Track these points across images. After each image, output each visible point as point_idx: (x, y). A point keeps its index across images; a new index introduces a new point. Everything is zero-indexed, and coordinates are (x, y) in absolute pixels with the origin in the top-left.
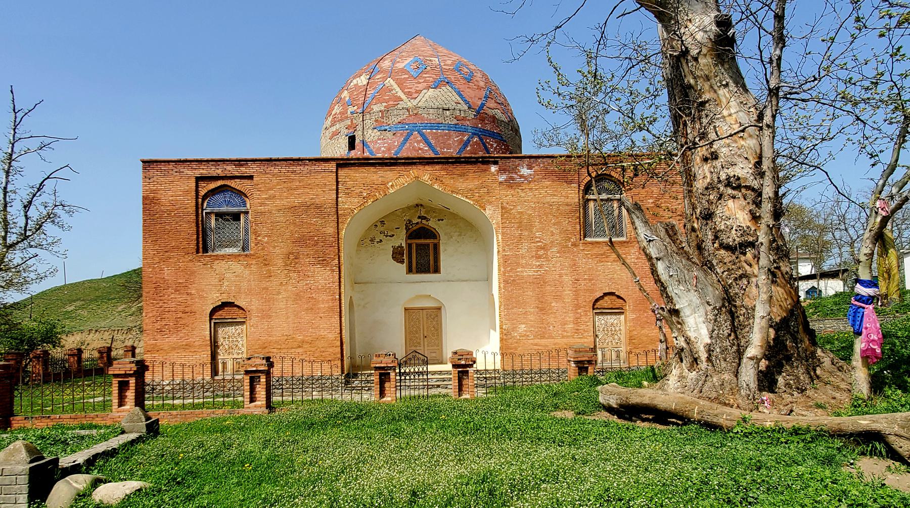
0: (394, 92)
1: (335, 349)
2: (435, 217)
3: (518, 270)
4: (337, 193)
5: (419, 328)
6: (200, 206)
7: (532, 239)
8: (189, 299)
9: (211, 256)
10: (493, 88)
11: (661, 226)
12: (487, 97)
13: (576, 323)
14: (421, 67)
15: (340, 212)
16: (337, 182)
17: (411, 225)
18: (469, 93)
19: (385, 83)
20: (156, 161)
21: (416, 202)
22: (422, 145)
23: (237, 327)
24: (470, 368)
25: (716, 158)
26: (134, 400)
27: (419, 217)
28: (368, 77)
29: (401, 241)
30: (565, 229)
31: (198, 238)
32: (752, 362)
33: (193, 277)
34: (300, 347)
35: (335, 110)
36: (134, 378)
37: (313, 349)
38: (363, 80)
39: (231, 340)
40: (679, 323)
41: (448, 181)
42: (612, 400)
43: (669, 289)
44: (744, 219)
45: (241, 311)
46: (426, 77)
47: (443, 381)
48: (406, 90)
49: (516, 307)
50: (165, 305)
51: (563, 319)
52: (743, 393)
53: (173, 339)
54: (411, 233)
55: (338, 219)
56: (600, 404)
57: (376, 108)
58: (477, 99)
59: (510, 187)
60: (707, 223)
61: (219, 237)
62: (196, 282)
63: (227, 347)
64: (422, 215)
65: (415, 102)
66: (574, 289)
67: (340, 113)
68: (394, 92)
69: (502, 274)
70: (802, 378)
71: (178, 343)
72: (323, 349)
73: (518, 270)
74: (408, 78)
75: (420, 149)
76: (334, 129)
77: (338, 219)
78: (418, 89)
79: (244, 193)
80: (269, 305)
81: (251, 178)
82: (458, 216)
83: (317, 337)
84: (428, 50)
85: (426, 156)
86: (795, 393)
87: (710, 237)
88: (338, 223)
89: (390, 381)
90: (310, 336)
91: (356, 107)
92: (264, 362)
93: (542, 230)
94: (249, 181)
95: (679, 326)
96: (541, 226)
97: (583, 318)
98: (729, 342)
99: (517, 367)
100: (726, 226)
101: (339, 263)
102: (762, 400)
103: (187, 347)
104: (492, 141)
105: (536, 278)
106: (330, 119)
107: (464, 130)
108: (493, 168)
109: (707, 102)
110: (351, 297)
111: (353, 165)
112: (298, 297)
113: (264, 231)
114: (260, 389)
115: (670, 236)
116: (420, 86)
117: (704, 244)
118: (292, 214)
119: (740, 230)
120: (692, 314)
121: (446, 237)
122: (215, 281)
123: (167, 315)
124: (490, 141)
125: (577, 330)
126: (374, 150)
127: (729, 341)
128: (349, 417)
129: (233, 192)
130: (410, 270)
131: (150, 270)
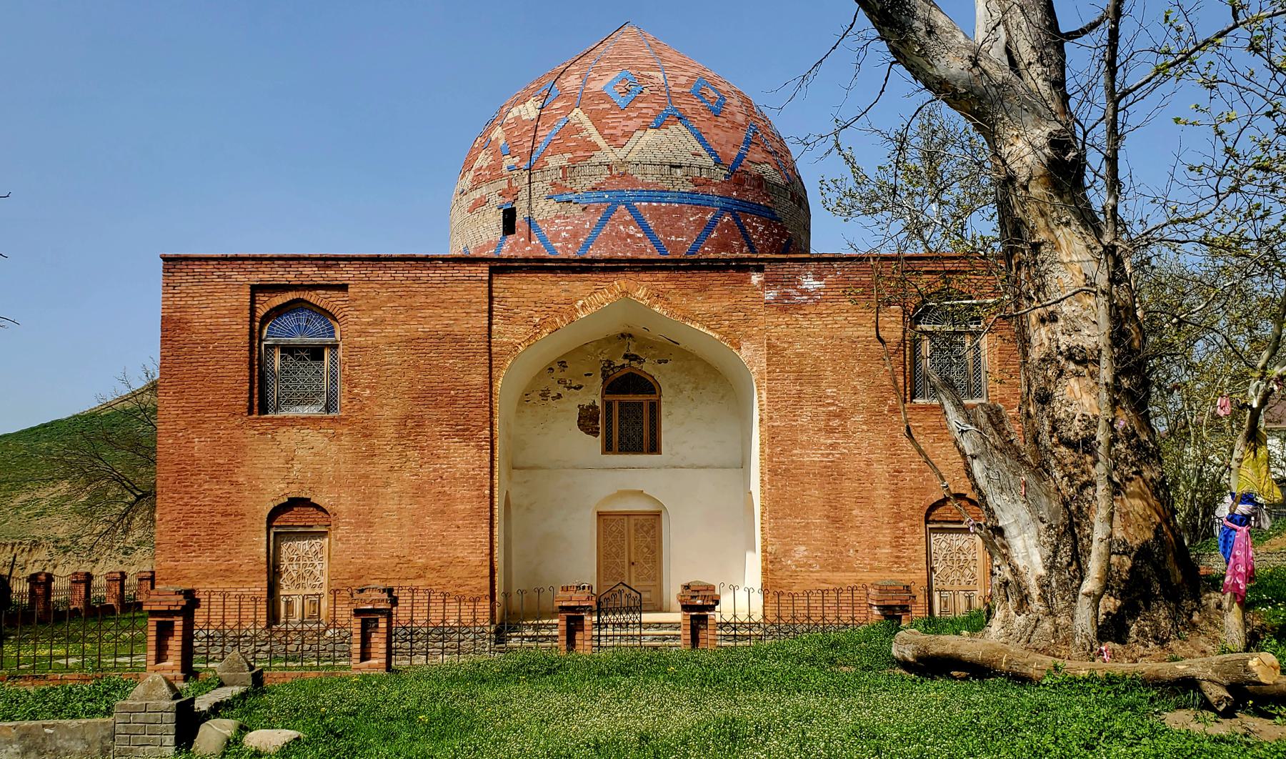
1: (480, 580)
2: (654, 356)
3: (795, 452)
4: (490, 318)
5: (622, 547)
6: (256, 335)
7: (819, 399)
8: (234, 491)
9: (273, 419)
10: (760, 124)
11: (982, 410)
12: (748, 142)
13: (897, 546)
14: (634, 90)
15: (494, 350)
16: (491, 298)
17: (612, 369)
18: (717, 136)
20: (186, 259)
21: (621, 330)
23: (313, 542)
24: (710, 611)
25: (1055, 320)
26: (180, 653)
27: (626, 357)
28: (540, 105)
29: (594, 397)
30: (878, 382)
31: (251, 388)
32: (1088, 600)
33: (242, 455)
34: (420, 577)
35: (479, 160)
36: (181, 618)
37: (443, 581)
38: (529, 110)
39: (301, 562)
40: (1004, 546)
41: (676, 299)
42: (907, 652)
44: (1091, 405)
45: (321, 514)
46: (641, 108)
47: (664, 640)
48: (606, 132)
49: (790, 515)
50: (194, 502)
51: (873, 538)
52: (1078, 641)
53: (206, 559)
54: (612, 384)
55: (491, 360)
56: (894, 658)
57: (553, 162)
58: (730, 146)
59: (784, 310)
60: (1043, 409)
61: (287, 387)
62: (246, 463)
63: (294, 575)
64: (632, 352)
65: (621, 153)
66: (893, 487)
67: (489, 167)
68: (585, 133)
69: (767, 458)
70: (1163, 624)
71: (212, 565)
72: (459, 581)
73: (795, 452)
74: (611, 109)
75: (629, 236)
76: (477, 194)
77: (491, 360)
78: (627, 129)
79: (331, 314)
80: (368, 505)
81: (343, 288)
82: (692, 354)
83: (450, 559)
84: (644, 55)
85: (642, 257)
86: (1151, 644)
87: (1046, 428)
89: (583, 630)
90: (439, 559)
91: (517, 159)
92: (385, 596)
94: (341, 294)
95: (1004, 551)
96: (835, 377)
97: (909, 538)
98: (1069, 574)
99: (787, 614)
100: (1066, 413)
101: (492, 435)
102: (1101, 651)
103: (228, 574)
104: (756, 222)
105: (825, 467)
106: (470, 176)
107: (707, 203)
108: (756, 278)
109: (1042, 243)
110: (507, 492)
111: (518, 270)
112: (419, 492)
113: (365, 378)
114: (376, 640)
115: (993, 424)
116: (632, 125)
117: (1040, 436)
118: (413, 352)
119: (1084, 420)
120: (1020, 535)
121: (672, 391)
122: (278, 463)
124: (753, 221)
125: (898, 557)
126: (549, 236)
127: (1069, 572)
128: (536, 672)
129: (313, 311)
130: (608, 448)
131: (170, 441)
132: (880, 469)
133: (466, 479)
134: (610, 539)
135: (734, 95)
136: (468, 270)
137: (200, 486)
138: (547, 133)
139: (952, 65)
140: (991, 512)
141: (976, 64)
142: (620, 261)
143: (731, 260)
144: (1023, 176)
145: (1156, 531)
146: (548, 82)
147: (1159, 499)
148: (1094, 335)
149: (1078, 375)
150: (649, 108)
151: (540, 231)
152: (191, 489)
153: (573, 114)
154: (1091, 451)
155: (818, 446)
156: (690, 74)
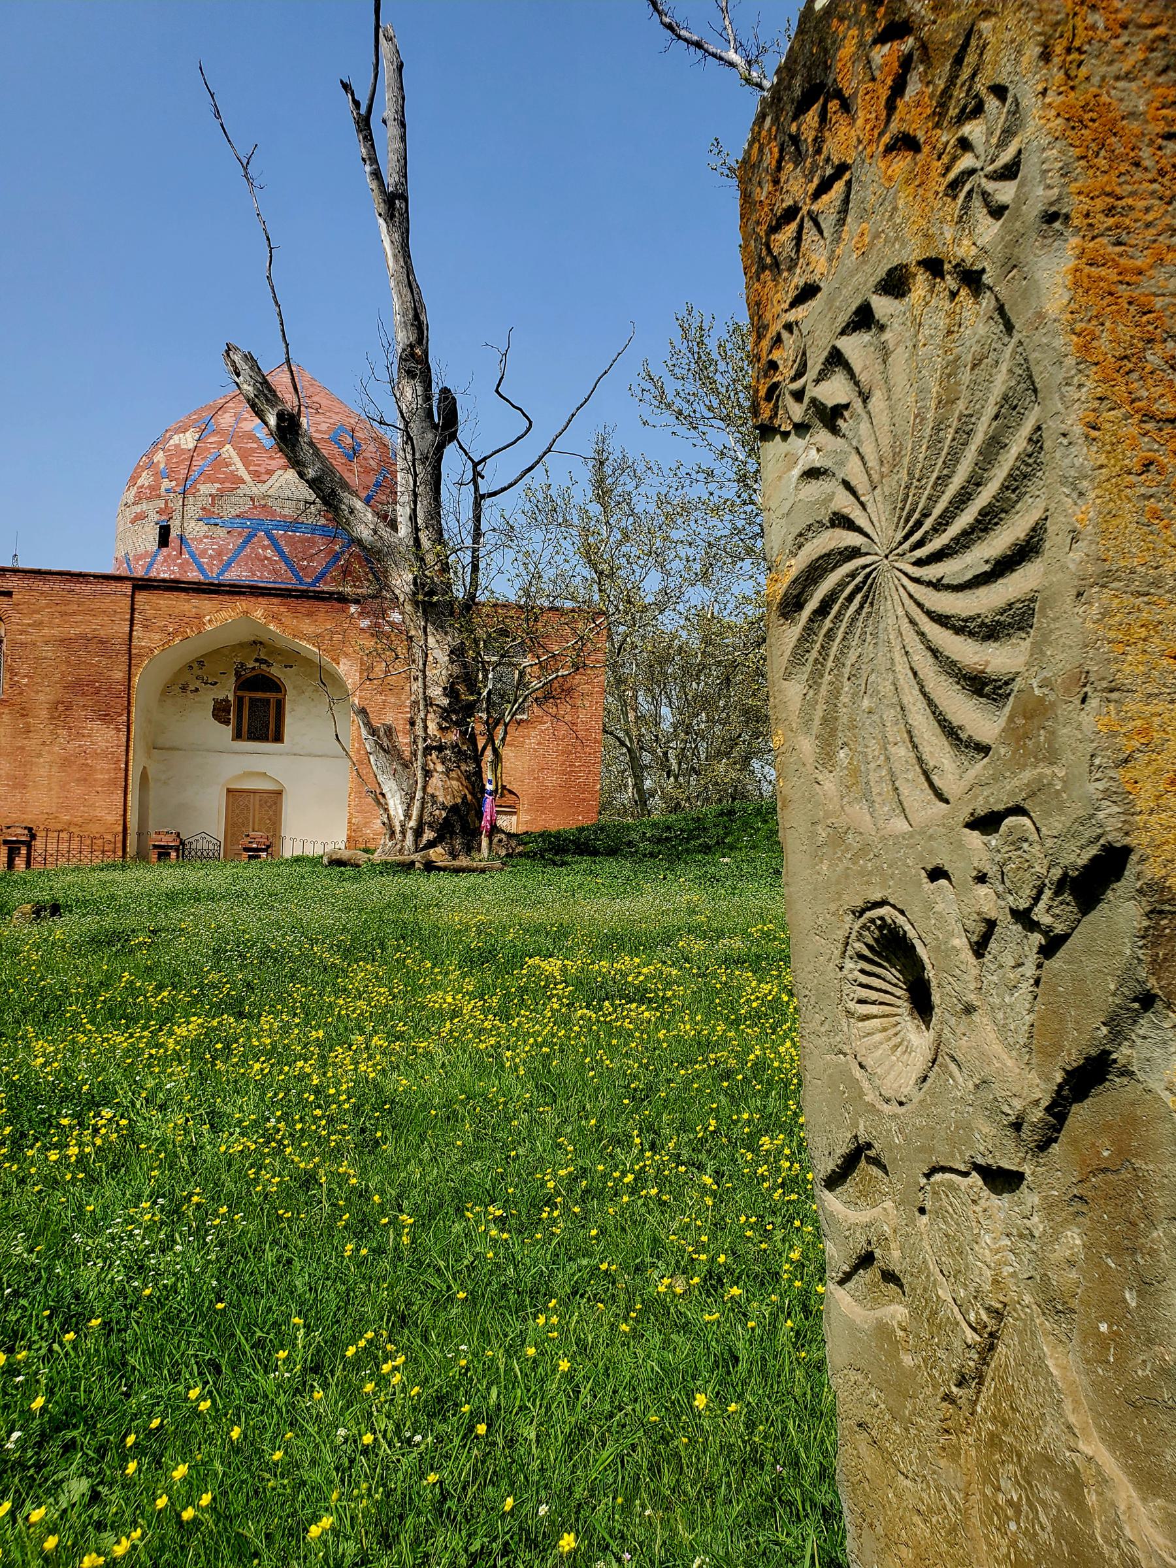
4: (132, 625)
5: (247, 819)
12: (378, 485)
15: (134, 651)
16: (133, 610)
22: (269, 553)
27: (257, 660)
38: (188, 440)
41: (288, 620)
48: (251, 468)
55: (130, 660)
65: (263, 488)
67: (149, 487)
75: (266, 558)
76: (137, 509)
77: (130, 660)
81: (9, 594)
88: (130, 666)
91: (174, 483)
92: (26, 832)
94: (6, 599)
101: (128, 720)
108: (353, 609)
112: (66, 763)
113: (24, 669)
130: (238, 736)
133: (105, 754)
136: (114, 586)
141: (375, 533)
142: (242, 587)
146: (207, 415)
151: (190, 546)
156: (331, 421)
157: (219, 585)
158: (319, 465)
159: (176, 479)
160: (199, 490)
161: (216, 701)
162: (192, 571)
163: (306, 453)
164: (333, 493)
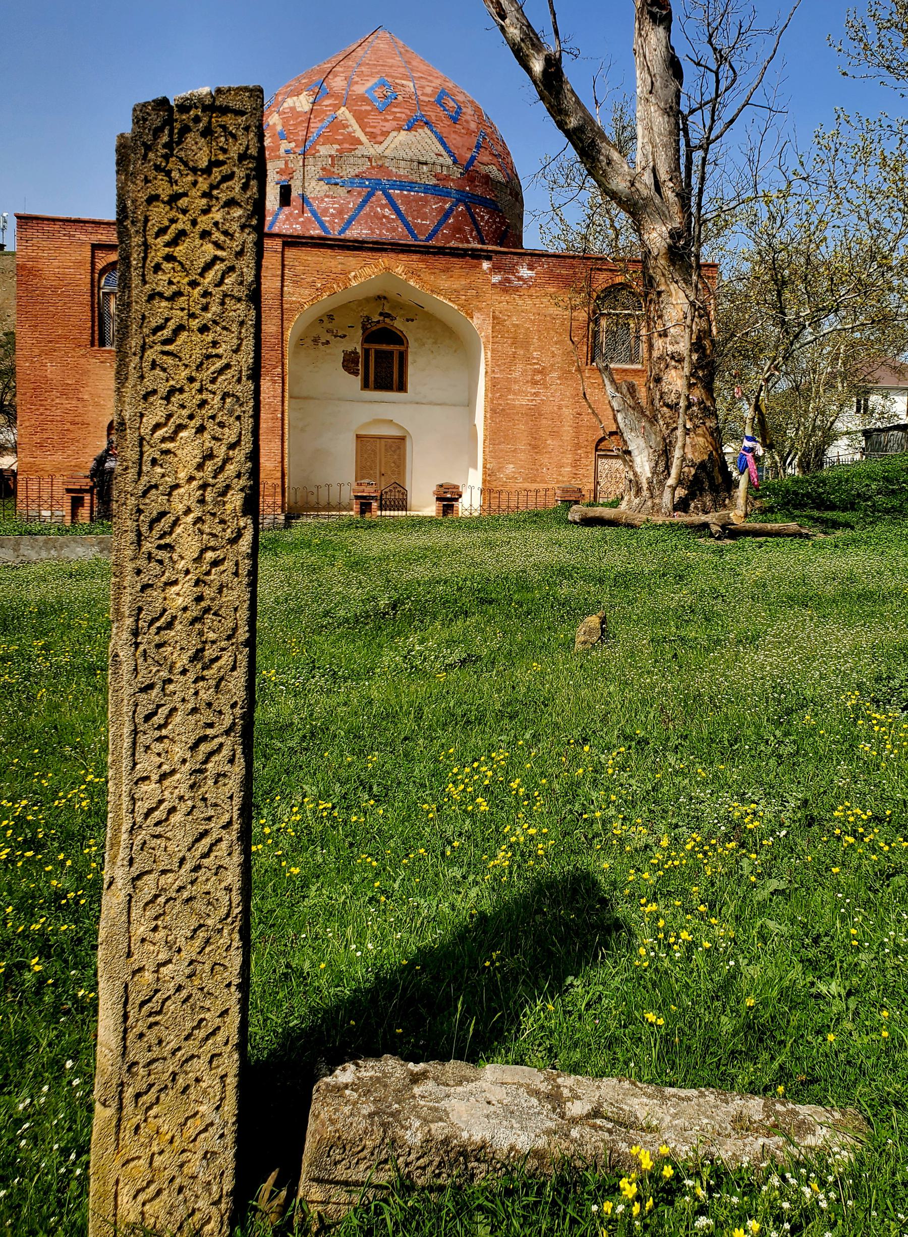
0: (350, 129)
4: (283, 281)
6: (96, 283)
7: (528, 360)
10: (489, 131)
12: (478, 147)
15: (285, 306)
16: (283, 266)
19: (337, 113)
20: (37, 218)
21: (379, 293)
22: (387, 212)
27: (381, 314)
28: (312, 100)
31: (93, 326)
40: (631, 461)
41: (426, 276)
43: (625, 435)
46: (396, 113)
48: (368, 130)
50: (48, 412)
53: (58, 457)
55: (282, 314)
59: (505, 291)
65: (379, 149)
66: (575, 425)
68: (350, 129)
69: (489, 401)
71: (64, 462)
74: (371, 111)
75: (384, 216)
77: (282, 314)
78: (384, 129)
88: (282, 320)
91: (293, 145)
93: (541, 348)
97: (584, 461)
101: (283, 372)
103: (76, 468)
108: (486, 265)
116: (388, 126)
123: (49, 426)
130: (366, 386)
132: (567, 412)
134: (365, 456)
135: (469, 105)
137: (53, 400)
138: (319, 125)
139: (619, 184)
140: (625, 442)
141: (633, 185)
143: (468, 250)
144: (655, 252)
145: (709, 456)
147: (713, 438)
148: (683, 347)
149: (675, 368)
150: (401, 113)
151: (311, 205)
152: (45, 403)
153: (340, 112)
154: (677, 410)
155: (526, 393)
156: (433, 85)
157: (363, 242)
158: (580, 114)
159: (295, 141)
160: (318, 151)
161: (346, 354)
162: (315, 229)
163: (569, 103)
164: (593, 144)
